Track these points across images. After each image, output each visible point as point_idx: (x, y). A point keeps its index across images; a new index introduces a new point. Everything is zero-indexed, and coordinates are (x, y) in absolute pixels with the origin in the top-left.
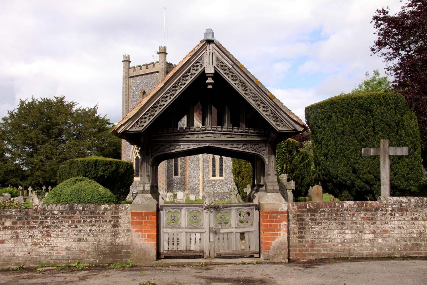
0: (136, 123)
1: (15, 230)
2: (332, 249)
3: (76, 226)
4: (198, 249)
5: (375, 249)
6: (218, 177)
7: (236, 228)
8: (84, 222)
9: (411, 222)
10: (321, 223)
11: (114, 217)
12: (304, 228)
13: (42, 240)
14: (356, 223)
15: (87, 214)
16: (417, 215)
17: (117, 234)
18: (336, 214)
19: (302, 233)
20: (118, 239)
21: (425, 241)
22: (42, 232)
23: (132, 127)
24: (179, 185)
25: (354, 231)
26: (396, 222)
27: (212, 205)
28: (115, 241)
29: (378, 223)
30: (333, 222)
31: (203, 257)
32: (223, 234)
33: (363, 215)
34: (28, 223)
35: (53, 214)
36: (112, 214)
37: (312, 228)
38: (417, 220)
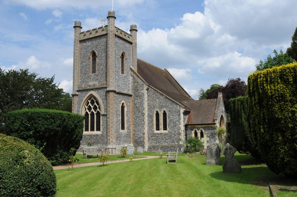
6: (162, 131)
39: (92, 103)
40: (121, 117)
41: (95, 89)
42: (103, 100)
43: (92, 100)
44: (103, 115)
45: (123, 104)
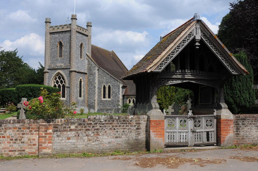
1: (77, 132)
2: (253, 140)
3: (115, 129)
6: (107, 99)
7: (205, 129)
8: (120, 126)
11: (137, 123)
12: (239, 129)
13: (94, 137)
15: (121, 121)
18: (255, 121)
19: (238, 132)
20: (140, 137)
22: (93, 132)
23: (155, 69)
24: (82, 103)
28: (138, 138)
30: (253, 125)
32: (198, 132)
34: (85, 127)
35: (101, 121)
36: (136, 121)
37: (243, 129)
39: (59, 78)
41: (61, 69)
42: (67, 76)
43: (59, 77)
44: (67, 87)
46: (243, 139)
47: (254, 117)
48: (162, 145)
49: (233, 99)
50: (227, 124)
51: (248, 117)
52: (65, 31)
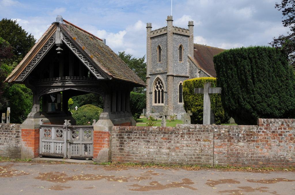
0: (19, 76)
4: (60, 153)
5: (170, 160)
7: (82, 141)
8: (2, 134)
9: (196, 142)
10: (134, 140)
11: (17, 131)
12: (123, 143)
14: (157, 142)
15: (4, 129)
16: (200, 137)
17: (19, 142)
18: (144, 135)
19: (122, 146)
20: (19, 145)
21: (204, 155)
23: (17, 79)
25: (155, 147)
26: (185, 142)
27: (69, 126)
29: (172, 142)
31: (62, 158)
32: (75, 144)
33: (162, 136)
37: (128, 143)
38: (200, 141)
39: (159, 83)
40: (179, 93)
41: (160, 73)
42: (165, 81)
43: (159, 82)
44: (165, 92)
45: (181, 84)
46: (129, 156)
47: (143, 130)
48: (32, 155)
49: (251, 105)
50: (101, 137)
51: (135, 130)
52: (164, 34)
